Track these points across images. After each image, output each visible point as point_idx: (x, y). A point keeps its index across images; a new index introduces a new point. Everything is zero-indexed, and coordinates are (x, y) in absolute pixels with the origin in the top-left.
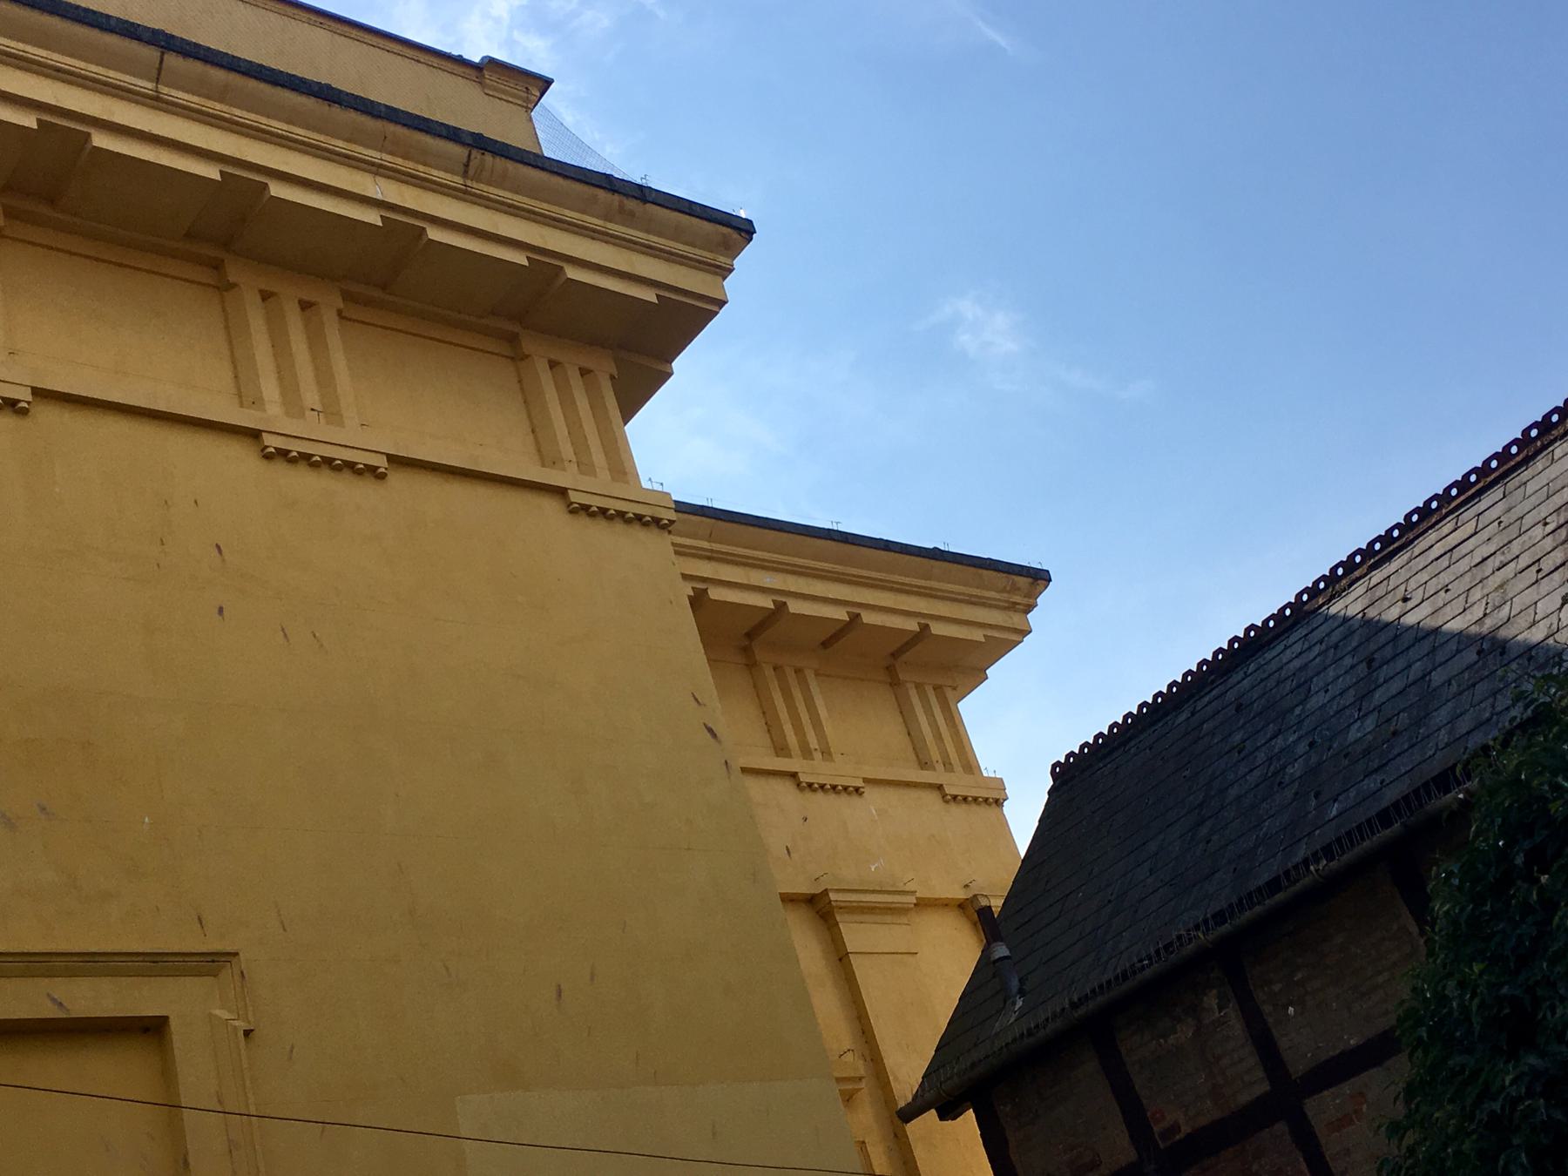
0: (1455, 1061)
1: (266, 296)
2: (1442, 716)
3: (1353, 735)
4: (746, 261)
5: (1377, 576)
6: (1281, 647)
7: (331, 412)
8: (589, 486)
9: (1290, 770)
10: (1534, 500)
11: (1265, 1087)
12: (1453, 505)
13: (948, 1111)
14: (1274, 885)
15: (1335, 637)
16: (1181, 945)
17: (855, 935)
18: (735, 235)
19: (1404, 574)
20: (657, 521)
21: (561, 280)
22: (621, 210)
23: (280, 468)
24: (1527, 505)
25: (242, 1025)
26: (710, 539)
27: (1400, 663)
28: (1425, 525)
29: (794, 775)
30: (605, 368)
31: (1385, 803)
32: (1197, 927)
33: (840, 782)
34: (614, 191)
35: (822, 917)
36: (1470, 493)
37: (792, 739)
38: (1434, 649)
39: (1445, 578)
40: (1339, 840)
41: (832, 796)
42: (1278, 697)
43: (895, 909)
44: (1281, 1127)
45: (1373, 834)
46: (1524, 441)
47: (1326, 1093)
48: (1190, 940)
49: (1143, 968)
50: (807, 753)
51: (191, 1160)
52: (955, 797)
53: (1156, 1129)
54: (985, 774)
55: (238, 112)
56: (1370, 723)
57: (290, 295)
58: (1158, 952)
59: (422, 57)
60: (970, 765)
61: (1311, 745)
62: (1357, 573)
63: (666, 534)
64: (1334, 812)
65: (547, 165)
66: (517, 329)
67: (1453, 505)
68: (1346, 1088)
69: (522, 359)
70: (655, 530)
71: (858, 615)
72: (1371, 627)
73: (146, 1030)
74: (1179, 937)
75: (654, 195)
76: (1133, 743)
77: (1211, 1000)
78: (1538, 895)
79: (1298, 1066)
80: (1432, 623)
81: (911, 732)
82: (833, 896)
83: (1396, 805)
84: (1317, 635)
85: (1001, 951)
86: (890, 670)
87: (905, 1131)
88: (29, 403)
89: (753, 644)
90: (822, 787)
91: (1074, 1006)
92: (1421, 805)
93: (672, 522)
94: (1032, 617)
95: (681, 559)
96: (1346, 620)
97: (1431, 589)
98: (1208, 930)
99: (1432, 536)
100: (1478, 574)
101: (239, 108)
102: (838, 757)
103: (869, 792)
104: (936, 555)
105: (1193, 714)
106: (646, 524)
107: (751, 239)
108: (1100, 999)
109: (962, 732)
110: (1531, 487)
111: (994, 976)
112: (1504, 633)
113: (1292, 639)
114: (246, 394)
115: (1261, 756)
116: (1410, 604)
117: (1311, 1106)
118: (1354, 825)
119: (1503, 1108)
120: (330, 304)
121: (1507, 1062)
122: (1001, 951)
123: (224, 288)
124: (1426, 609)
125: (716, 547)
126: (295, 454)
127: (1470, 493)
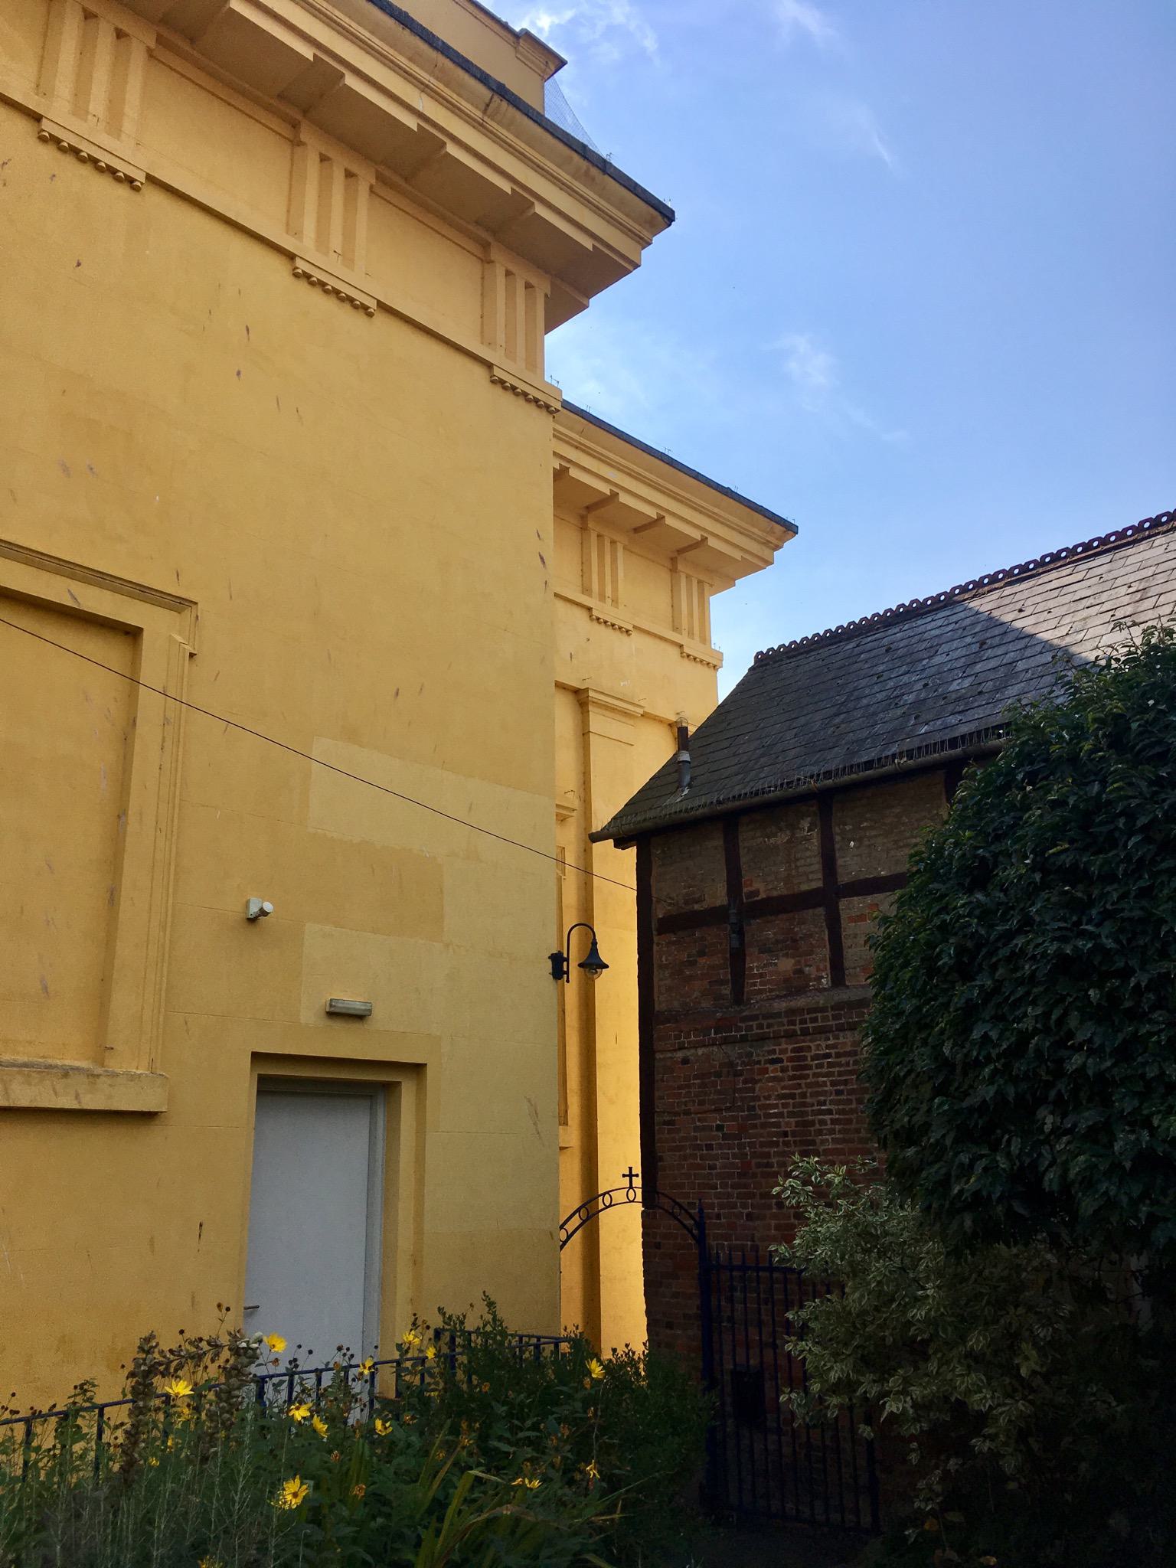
0: (935, 886)
1: (323, 159)
2: (1012, 691)
3: (954, 686)
4: (662, 240)
5: (1009, 590)
6: (930, 619)
7: (347, 257)
8: (509, 368)
9: (905, 697)
10: (1129, 569)
11: (820, 884)
12: (1076, 558)
13: (621, 843)
14: (869, 765)
15: (967, 622)
16: (798, 784)
17: (598, 721)
18: (660, 218)
19: (1026, 594)
20: (547, 407)
21: (532, 212)
22: (587, 173)
23: (302, 286)
24: (1123, 571)
25: (189, 649)
26: (581, 433)
27: (1000, 651)
28: (1052, 566)
29: (590, 609)
30: (543, 287)
31: (957, 734)
32: (812, 777)
33: (618, 623)
34: (585, 158)
35: (580, 704)
36: (1090, 553)
37: (595, 587)
38: (1026, 647)
39: (1051, 604)
40: (919, 748)
41: (610, 631)
42: (916, 650)
43: (629, 714)
44: (821, 911)
45: (942, 750)
46: (1138, 529)
47: (855, 898)
48: (805, 783)
49: (770, 791)
50: (602, 597)
51: (138, 721)
52: (688, 656)
53: (745, 890)
54: (713, 647)
55: (337, 13)
56: (967, 683)
57: (341, 162)
58: (782, 785)
59: (481, 16)
60: (705, 639)
61: (926, 685)
62: (997, 585)
63: (551, 418)
64: (923, 731)
65: (544, 124)
66: (490, 239)
67: (1076, 558)
68: (869, 899)
69: (488, 263)
70: (544, 413)
71: (664, 517)
72: (992, 623)
73: (127, 633)
74: (799, 780)
75: (612, 170)
76: (813, 653)
77: (805, 824)
78: (1021, 798)
79: (843, 879)
80: (1031, 630)
81: (674, 607)
82: (591, 694)
83: (963, 737)
84: (954, 618)
85: (685, 757)
86: (673, 560)
87: (591, 848)
88: (142, 184)
89: (589, 515)
90: (605, 622)
91: (719, 802)
92: (979, 742)
93: (558, 411)
94: (646, 253)
95: (555, 439)
96: (977, 613)
97: (1040, 608)
98: (818, 780)
99: (1054, 574)
100: (1074, 607)
101: (339, 10)
102: (621, 607)
103: (634, 634)
104: (727, 492)
105: (858, 646)
106: (539, 407)
107: (670, 225)
108: (737, 803)
109: (707, 613)
110: (1130, 560)
111: (676, 772)
112: (1074, 649)
113: (939, 616)
114: (292, 228)
115: (891, 684)
116: (1022, 614)
117: (843, 904)
118: (932, 742)
119: (951, 919)
120: (366, 177)
121: (964, 894)
122: (685, 757)
123: (296, 143)
124: (1032, 620)
125: (583, 441)
126: (315, 279)
127: (1090, 553)
